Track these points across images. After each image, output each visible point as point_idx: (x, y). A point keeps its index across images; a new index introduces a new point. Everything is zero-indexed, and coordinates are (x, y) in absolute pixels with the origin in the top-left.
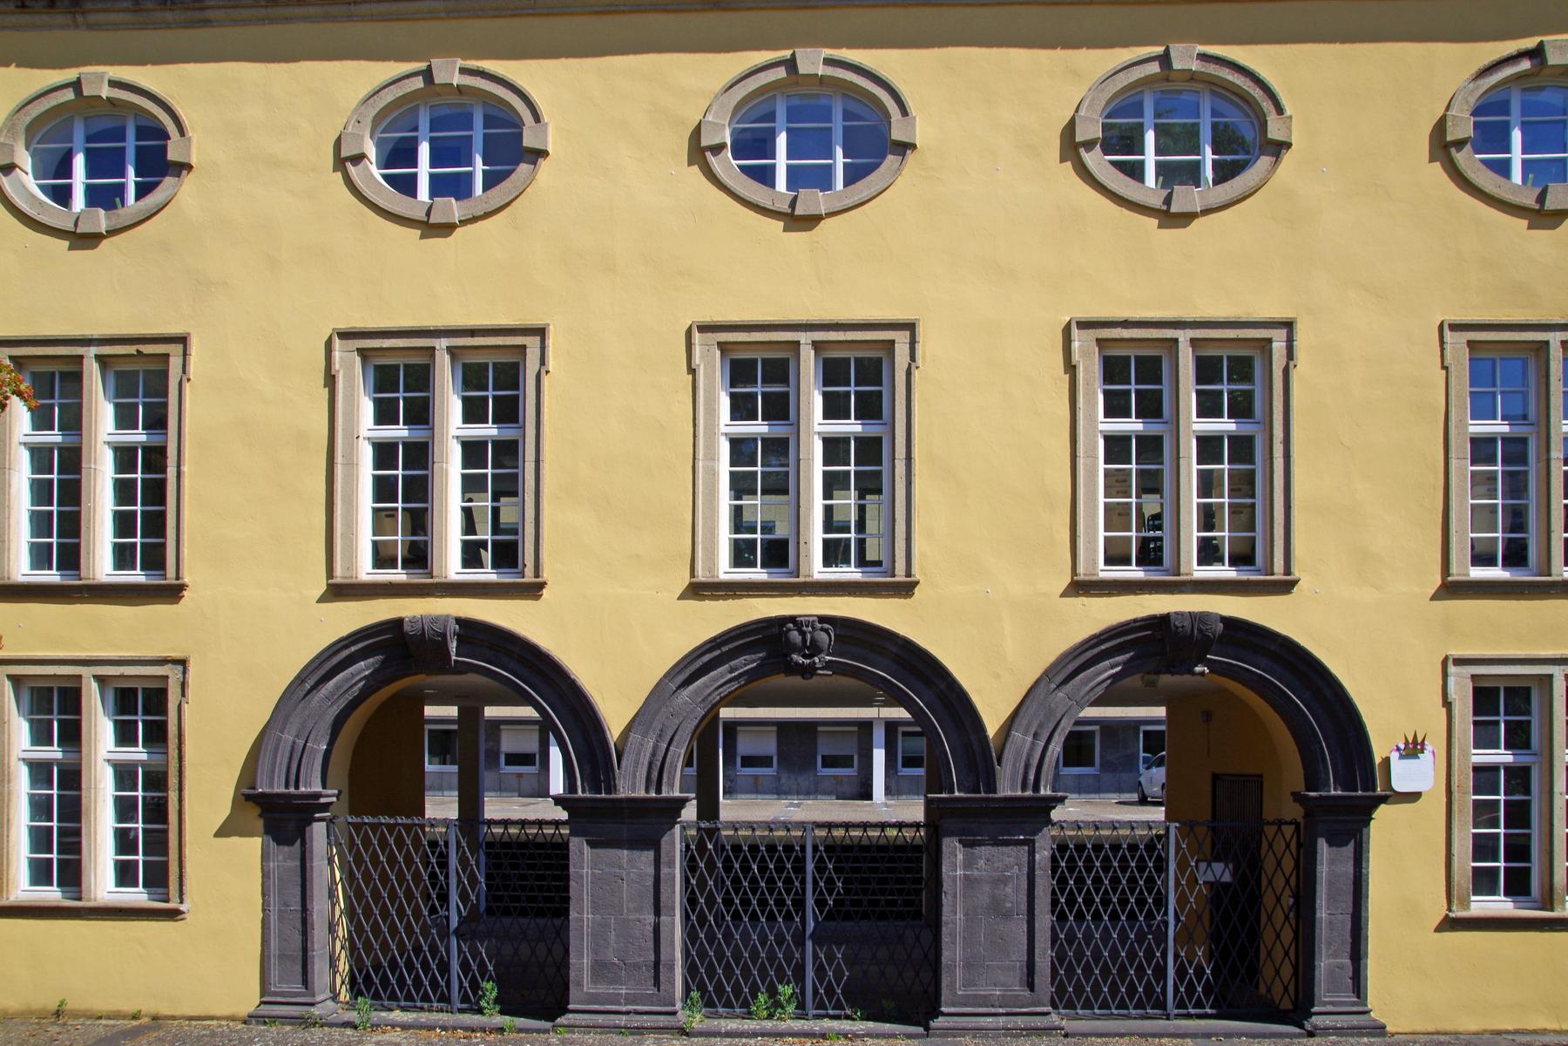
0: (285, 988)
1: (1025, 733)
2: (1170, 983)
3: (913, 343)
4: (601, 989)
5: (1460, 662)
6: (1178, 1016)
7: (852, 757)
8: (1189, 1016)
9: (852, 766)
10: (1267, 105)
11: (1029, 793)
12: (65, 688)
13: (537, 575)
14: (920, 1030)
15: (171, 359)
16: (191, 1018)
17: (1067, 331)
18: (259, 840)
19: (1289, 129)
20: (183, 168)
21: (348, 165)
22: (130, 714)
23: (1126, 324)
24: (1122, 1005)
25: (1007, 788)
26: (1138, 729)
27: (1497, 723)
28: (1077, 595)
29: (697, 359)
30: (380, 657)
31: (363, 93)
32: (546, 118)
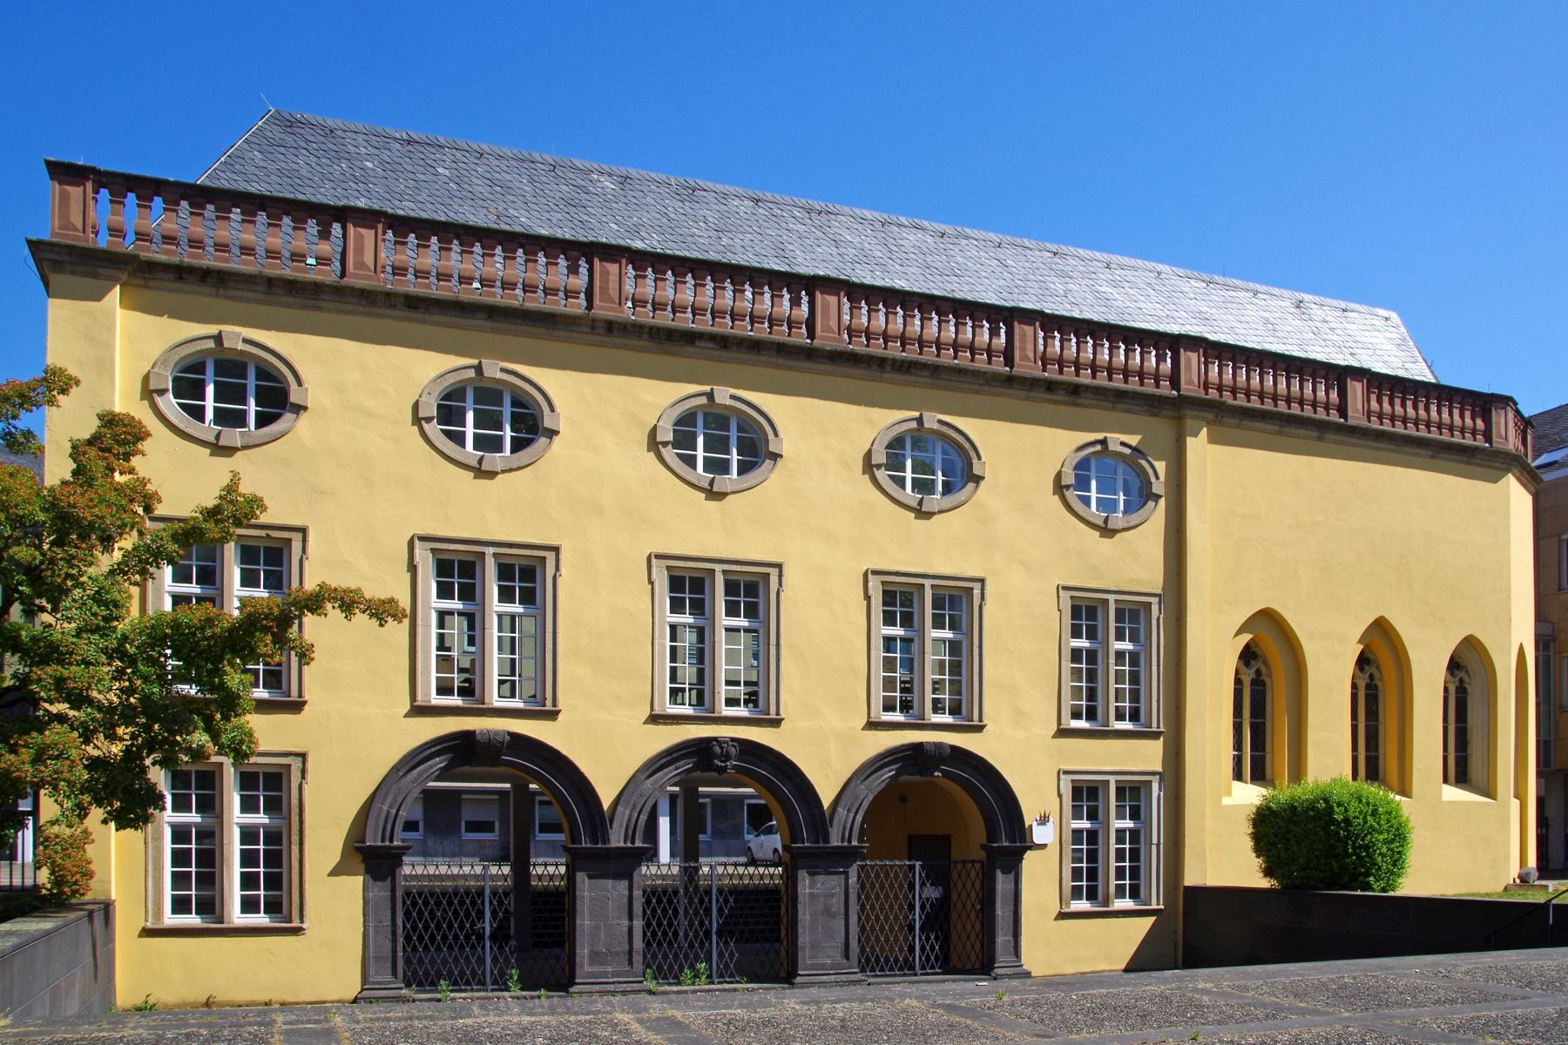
0: (380, 979)
1: (626, 808)
2: (917, 955)
3: (780, 576)
4: (595, 969)
5: (1066, 772)
6: (922, 974)
7: (493, 823)
8: (927, 974)
9: (417, 830)
10: (972, 454)
11: (846, 844)
12: (203, 772)
13: (554, 705)
14: (563, 994)
15: (293, 542)
16: (310, 1003)
17: (866, 575)
18: (361, 878)
20: (299, 409)
21: (423, 422)
22: (209, 790)
23: (898, 574)
24: (892, 969)
25: (617, 840)
26: (743, 802)
27: (1082, 806)
28: (870, 729)
29: (654, 576)
30: (451, 755)
31: (433, 375)
32: (558, 409)
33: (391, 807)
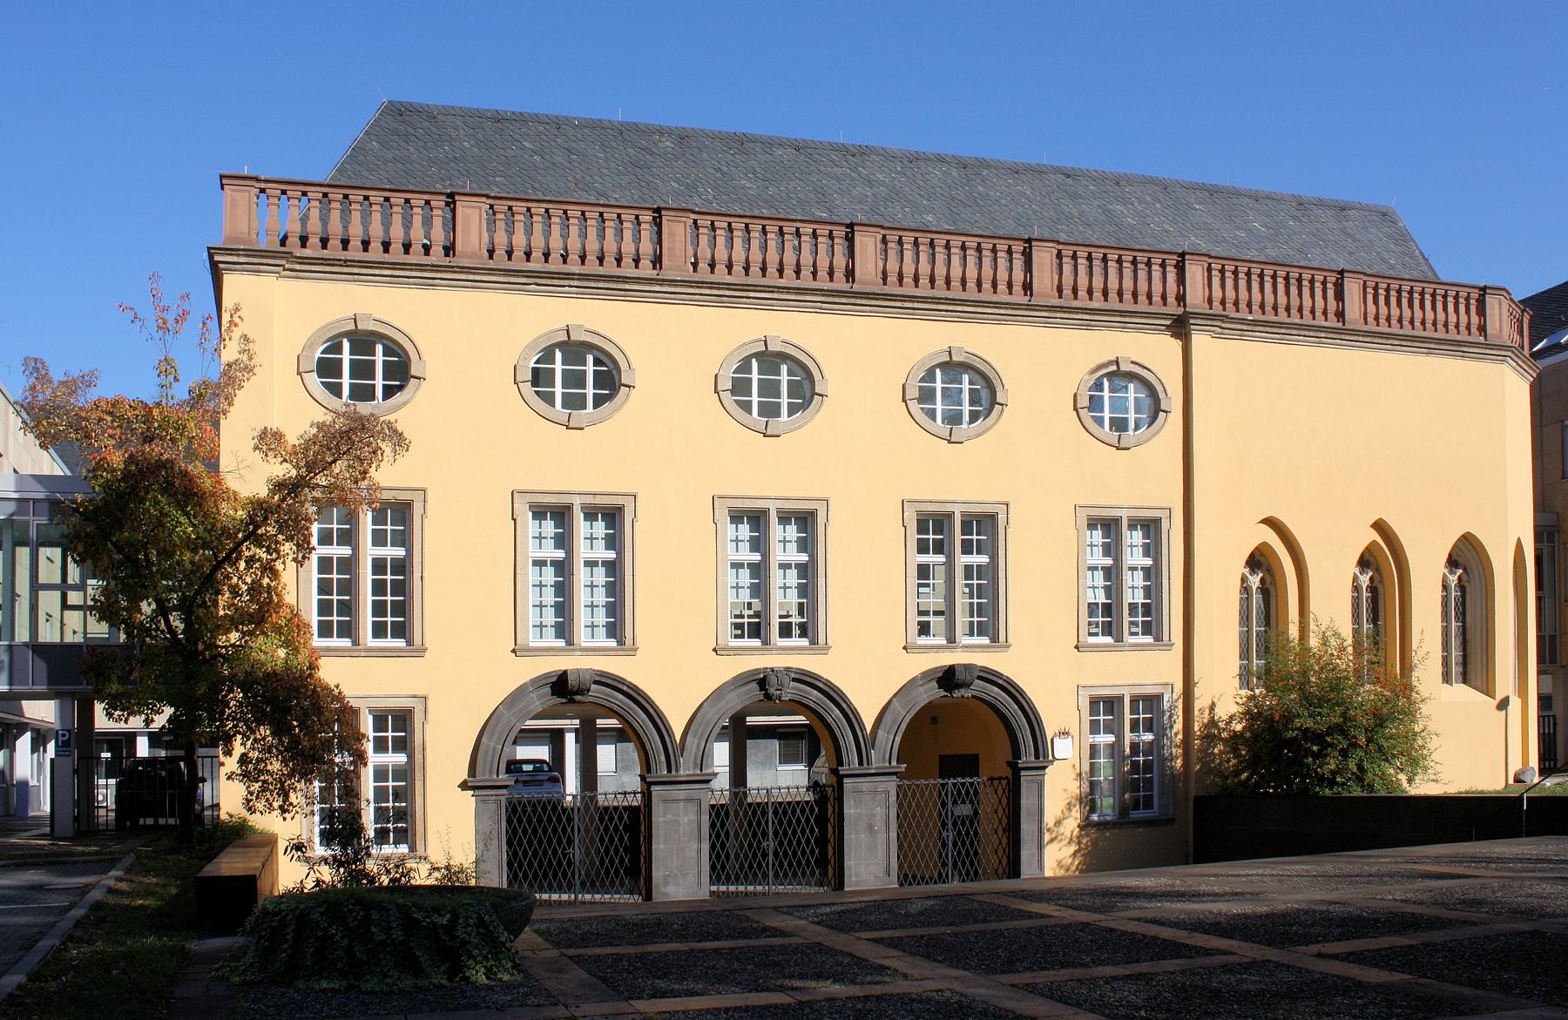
1: (694, 737)
19: (1007, 396)
33: (497, 743)
